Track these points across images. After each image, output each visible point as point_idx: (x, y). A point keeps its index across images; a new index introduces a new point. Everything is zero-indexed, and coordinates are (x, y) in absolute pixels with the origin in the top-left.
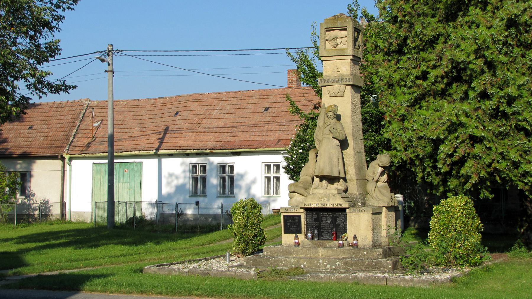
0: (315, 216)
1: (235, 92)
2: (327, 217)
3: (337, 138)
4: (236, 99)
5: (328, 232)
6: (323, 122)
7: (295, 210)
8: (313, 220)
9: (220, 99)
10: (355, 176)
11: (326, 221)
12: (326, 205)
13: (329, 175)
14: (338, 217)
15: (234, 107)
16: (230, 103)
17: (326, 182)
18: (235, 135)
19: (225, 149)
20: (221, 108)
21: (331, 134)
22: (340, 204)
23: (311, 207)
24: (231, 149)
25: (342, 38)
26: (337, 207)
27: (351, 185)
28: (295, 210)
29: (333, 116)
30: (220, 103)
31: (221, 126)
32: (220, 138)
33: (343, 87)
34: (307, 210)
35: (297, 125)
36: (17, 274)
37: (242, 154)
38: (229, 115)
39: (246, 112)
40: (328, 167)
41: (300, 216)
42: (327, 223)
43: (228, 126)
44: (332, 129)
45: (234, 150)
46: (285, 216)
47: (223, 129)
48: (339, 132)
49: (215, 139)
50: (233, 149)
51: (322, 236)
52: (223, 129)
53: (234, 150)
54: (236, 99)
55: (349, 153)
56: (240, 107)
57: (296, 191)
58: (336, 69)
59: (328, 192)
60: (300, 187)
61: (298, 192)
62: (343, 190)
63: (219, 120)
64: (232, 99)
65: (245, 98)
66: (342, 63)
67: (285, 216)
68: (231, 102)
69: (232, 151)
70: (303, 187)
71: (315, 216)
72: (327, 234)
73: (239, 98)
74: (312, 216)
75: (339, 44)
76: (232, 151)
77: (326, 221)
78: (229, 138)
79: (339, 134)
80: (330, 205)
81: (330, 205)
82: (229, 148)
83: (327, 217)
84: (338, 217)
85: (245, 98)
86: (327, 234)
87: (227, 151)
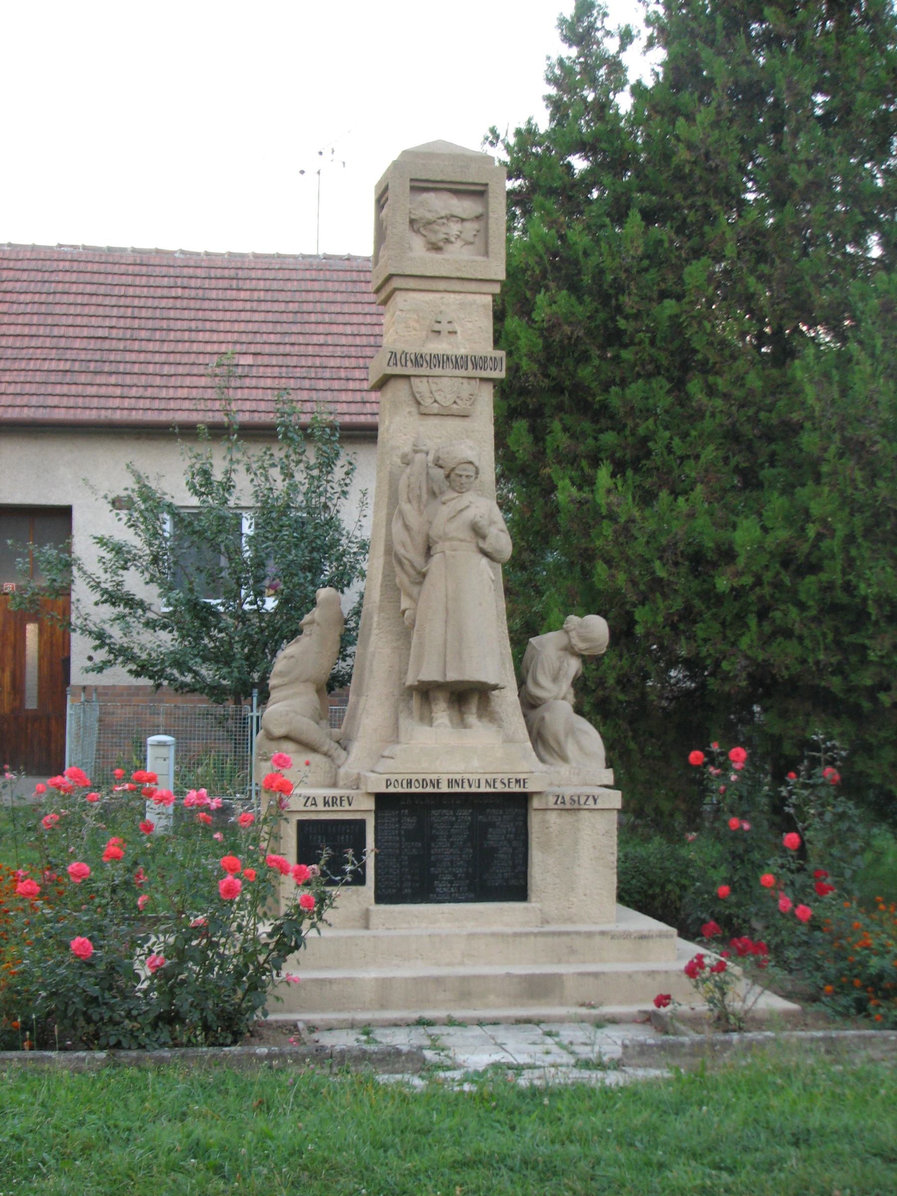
0: (410, 822)
2: (452, 824)
5: (455, 875)
7: (345, 803)
8: (399, 835)
11: (449, 836)
12: (466, 784)
14: (493, 825)
22: (518, 781)
23: (413, 790)
25: (463, 220)
26: (507, 790)
28: (345, 803)
33: (467, 388)
34: (384, 801)
35: (191, 590)
36: (186, 689)
41: (362, 823)
42: (452, 843)
46: (301, 824)
51: (433, 892)
58: (444, 323)
66: (462, 305)
67: (301, 824)
71: (410, 822)
72: (451, 882)
74: (399, 821)
75: (453, 239)
77: (449, 836)
80: (483, 783)
81: (483, 783)
83: (452, 824)
84: (493, 825)
86: (451, 882)
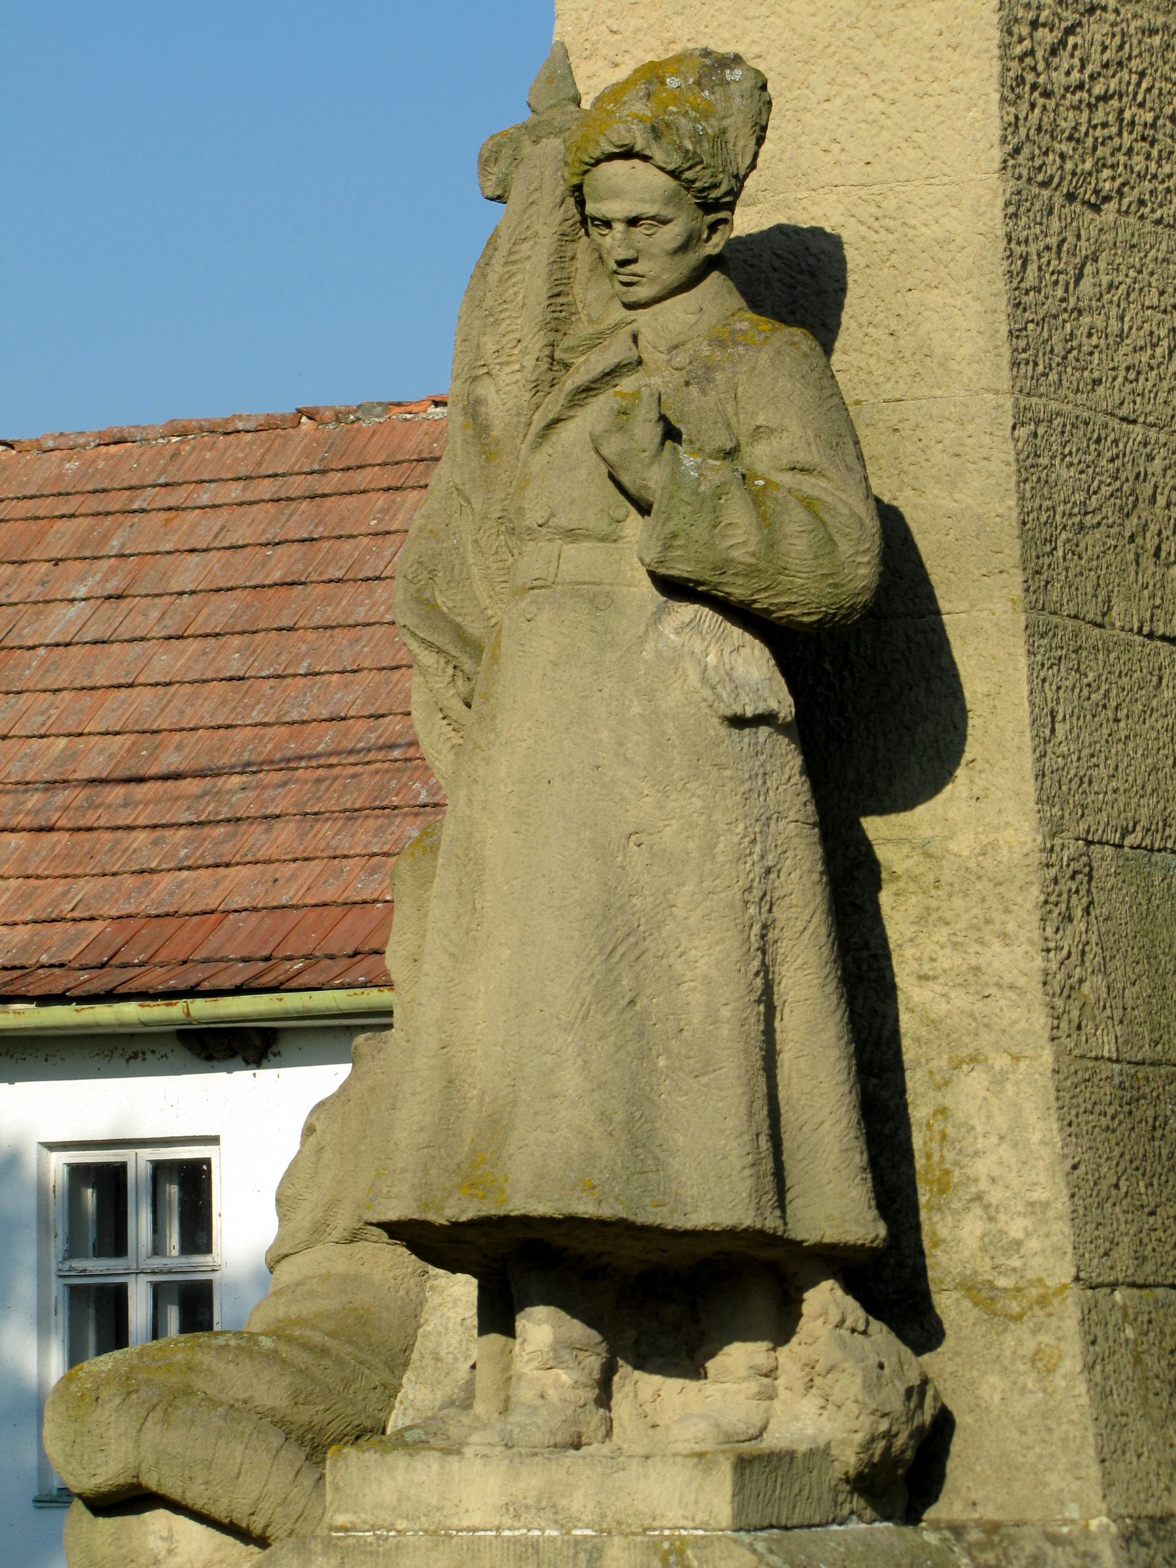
1: (269, 426)
3: (738, 591)
4: (267, 488)
6: (536, 344)
9: (117, 501)
10: (1061, 1231)
13: (585, 1208)
15: (243, 569)
16: (205, 528)
17: (577, 1329)
18: (227, 851)
19: (110, 997)
20: (111, 587)
21: (635, 524)
24: (171, 995)
27: (992, 1387)
29: (671, 234)
30: (107, 537)
31: (96, 765)
32: (84, 889)
37: (284, 1046)
38: (193, 646)
39: (360, 615)
40: (571, 1081)
43: (171, 760)
44: (647, 432)
45: (202, 1009)
47: (120, 791)
48: (757, 499)
49: (27, 897)
50: (192, 993)
52: (117, 793)
53: (202, 1009)
54: (267, 488)
55: (962, 845)
56: (297, 571)
57: (172, 1488)
59: (580, 1502)
60: (236, 1410)
61: (195, 1497)
62: (849, 1459)
63: (87, 699)
64: (235, 492)
65: (360, 479)
68: (215, 521)
69: (175, 1011)
70: (280, 1423)
73: (299, 486)
76: (175, 1011)
78: (166, 881)
79: (767, 522)
82: (154, 979)
85: (360, 479)
87: (130, 1011)
